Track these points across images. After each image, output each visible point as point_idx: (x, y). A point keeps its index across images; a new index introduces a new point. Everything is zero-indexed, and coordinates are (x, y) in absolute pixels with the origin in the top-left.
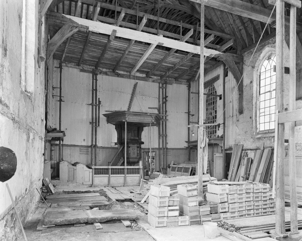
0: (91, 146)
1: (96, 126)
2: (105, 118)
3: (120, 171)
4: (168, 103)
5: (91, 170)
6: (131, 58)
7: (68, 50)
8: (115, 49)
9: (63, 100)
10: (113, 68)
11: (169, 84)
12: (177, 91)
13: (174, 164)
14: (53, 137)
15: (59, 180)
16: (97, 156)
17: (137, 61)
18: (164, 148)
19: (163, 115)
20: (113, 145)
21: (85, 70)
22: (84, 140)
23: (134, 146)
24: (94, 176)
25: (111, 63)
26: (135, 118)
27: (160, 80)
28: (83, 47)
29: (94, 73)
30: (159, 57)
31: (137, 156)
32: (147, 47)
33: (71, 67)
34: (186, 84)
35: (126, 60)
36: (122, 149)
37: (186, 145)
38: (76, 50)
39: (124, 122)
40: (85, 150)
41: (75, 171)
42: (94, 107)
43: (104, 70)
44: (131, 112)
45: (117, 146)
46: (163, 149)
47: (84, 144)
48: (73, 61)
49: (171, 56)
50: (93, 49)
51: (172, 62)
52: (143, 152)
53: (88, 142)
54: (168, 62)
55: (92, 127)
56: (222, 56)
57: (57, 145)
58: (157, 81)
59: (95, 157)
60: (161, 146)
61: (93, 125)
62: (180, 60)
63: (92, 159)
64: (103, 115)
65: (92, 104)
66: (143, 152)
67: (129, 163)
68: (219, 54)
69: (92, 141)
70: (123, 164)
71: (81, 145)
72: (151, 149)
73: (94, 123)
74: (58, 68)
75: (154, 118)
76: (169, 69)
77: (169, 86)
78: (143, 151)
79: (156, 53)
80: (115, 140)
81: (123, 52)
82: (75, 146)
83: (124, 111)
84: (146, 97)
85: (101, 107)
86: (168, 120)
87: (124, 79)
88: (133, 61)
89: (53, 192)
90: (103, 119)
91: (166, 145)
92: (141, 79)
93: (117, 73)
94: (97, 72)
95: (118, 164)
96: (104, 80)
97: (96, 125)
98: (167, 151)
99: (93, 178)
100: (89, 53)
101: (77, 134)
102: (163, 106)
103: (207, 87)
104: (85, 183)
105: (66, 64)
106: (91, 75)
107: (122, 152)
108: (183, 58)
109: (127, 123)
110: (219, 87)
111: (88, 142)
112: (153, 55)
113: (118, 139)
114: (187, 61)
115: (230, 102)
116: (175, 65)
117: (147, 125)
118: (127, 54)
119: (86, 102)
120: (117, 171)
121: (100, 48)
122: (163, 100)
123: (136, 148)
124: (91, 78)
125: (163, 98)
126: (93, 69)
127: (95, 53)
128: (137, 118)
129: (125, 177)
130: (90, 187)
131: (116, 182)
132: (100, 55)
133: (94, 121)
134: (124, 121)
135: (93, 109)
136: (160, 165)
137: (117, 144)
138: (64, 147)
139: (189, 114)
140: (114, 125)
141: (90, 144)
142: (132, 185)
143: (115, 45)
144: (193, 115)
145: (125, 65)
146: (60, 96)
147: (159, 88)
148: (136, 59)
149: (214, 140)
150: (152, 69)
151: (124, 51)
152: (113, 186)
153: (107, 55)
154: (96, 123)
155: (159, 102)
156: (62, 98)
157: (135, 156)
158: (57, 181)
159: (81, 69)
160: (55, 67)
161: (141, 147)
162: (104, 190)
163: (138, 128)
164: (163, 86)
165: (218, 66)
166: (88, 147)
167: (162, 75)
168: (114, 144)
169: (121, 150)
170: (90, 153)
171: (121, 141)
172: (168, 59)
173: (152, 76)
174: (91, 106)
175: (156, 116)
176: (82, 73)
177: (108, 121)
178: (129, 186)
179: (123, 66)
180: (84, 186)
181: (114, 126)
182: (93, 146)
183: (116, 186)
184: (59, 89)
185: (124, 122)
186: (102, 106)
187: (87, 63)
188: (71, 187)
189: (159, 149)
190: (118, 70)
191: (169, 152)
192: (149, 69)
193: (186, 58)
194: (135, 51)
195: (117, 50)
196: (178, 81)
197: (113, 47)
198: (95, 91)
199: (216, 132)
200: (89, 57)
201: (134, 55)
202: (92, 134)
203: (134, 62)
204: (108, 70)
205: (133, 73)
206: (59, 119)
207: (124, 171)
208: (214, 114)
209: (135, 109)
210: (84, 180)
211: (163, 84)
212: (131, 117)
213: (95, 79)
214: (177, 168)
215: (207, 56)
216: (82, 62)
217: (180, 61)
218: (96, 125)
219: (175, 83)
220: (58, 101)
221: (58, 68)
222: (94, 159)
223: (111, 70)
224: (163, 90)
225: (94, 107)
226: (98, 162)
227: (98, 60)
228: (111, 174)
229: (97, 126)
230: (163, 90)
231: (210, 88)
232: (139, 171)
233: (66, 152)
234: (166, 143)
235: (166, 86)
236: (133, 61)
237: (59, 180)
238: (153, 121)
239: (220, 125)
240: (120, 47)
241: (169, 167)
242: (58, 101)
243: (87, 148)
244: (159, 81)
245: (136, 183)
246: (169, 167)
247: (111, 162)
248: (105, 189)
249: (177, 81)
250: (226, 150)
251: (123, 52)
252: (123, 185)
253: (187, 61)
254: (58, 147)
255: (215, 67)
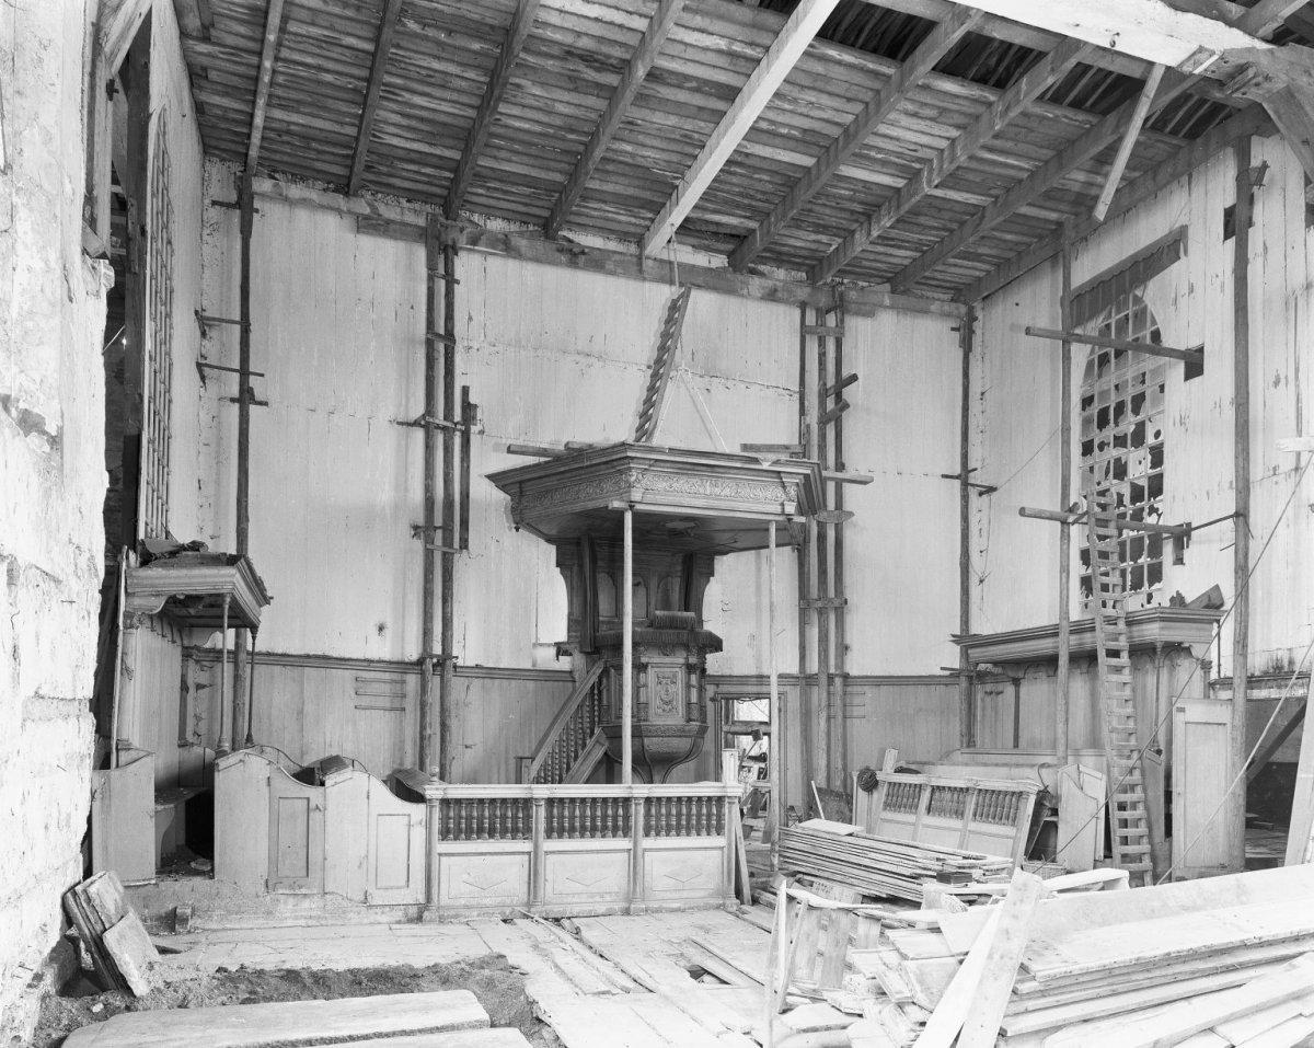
0: (420, 662)
1: (451, 545)
2: (500, 497)
3: (604, 817)
4: (850, 422)
5: (417, 811)
6: (662, 134)
7: (280, 79)
8: (569, 53)
9: (259, 396)
10: (546, 214)
11: (857, 314)
12: (896, 351)
13: (900, 770)
14: (173, 590)
15: (210, 874)
16: (453, 723)
17: (691, 148)
18: (831, 678)
19: (839, 475)
20: (546, 659)
21: (389, 222)
22: (381, 629)
23: (667, 660)
24: (442, 847)
25: (534, 173)
26: (686, 487)
27: (808, 290)
28: (369, 47)
29: (438, 238)
30: (830, 112)
31: (689, 720)
32: (768, 30)
33: (304, 202)
34: (949, 315)
35: (629, 148)
36: (600, 678)
37: (952, 658)
38: (329, 78)
39: (620, 514)
40: (386, 688)
41: (315, 816)
42: (440, 438)
43: (496, 225)
44: (659, 450)
45: (565, 663)
46: (823, 680)
47: (382, 649)
48: (318, 165)
49: (910, 107)
50: (436, 65)
51: (899, 155)
52: (713, 700)
53: (401, 638)
54: (880, 150)
55: (429, 554)
56: (1264, 61)
57: (217, 654)
58: (790, 292)
59: (444, 726)
60: (813, 666)
61: (429, 540)
62: (954, 133)
63: (422, 738)
64: (491, 477)
65: (425, 424)
66: (713, 700)
67: (651, 765)
68: (1250, 50)
69: (427, 633)
70: (608, 770)
71: (361, 657)
72: (774, 679)
73: (439, 533)
74: (228, 206)
75: (793, 491)
76: (872, 204)
77: (857, 326)
78: (710, 690)
79: (817, 84)
80: (556, 626)
81: (611, 79)
82: (325, 661)
83: (623, 444)
84: (729, 384)
85: (475, 440)
86: (851, 514)
87: (611, 280)
88: (665, 156)
89: (139, 986)
90: (487, 497)
91: (841, 663)
92: (700, 281)
93: (570, 241)
94: (452, 235)
95: (575, 766)
96: (498, 288)
97: (448, 541)
98: (845, 693)
99: (435, 859)
100: (407, 96)
101: (338, 602)
102: (823, 437)
103: (1093, 316)
104: (378, 898)
105: (275, 185)
106: (421, 253)
107: (600, 700)
108: (977, 118)
109: (639, 518)
110: (1183, 302)
111: (401, 638)
112: (795, 101)
113: (573, 623)
114: (998, 143)
115: (1276, 383)
116: (913, 176)
117: (743, 540)
118: (642, 99)
119: (388, 410)
120: (583, 817)
121: (476, 46)
122: (822, 404)
123: (681, 674)
124: (423, 271)
125: (823, 394)
126: (433, 219)
127: (448, 95)
128: (693, 489)
129: (634, 857)
130: (410, 921)
131: (578, 888)
132: (472, 113)
133: (438, 521)
134: (616, 504)
135: (429, 448)
136: (809, 774)
137: (567, 653)
138: (261, 671)
139: (965, 485)
140: (549, 540)
141: (413, 653)
142: (675, 905)
143: (570, 23)
144: (991, 490)
145: (619, 189)
146: (244, 372)
147: (804, 331)
148: (687, 139)
149: (1163, 620)
150: (768, 215)
151: (623, 68)
152: (556, 911)
153: (516, 111)
154: (447, 529)
155: (802, 411)
156: (253, 381)
157: (676, 719)
158: (197, 881)
159: (366, 218)
160: (214, 203)
161: (704, 670)
162: (511, 961)
163: (686, 551)
164: (821, 322)
165: (1175, 177)
166: (402, 666)
167: (820, 260)
168: (553, 651)
169: (593, 688)
170: (411, 704)
171: (593, 638)
172: (883, 129)
173: (762, 268)
174: (419, 434)
175: (807, 476)
176: (367, 242)
177: (521, 518)
178: (658, 910)
179: (603, 197)
180: (372, 916)
181: (552, 549)
182: (429, 665)
183: (576, 910)
184: (237, 329)
185: (620, 514)
186: (482, 432)
187: (397, 182)
188: (289, 923)
189: (806, 680)
190: (572, 225)
191: (857, 700)
192: (754, 213)
193: (1007, 109)
194: (690, 69)
195: (581, 67)
196: (906, 292)
197: (558, 37)
198: (441, 347)
199: (1156, 574)
200: (409, 128)
201: (678, 104)
202: (428, 594)
203: (675, 158)
204: (514, 227)
205: (657, 245)
206: (239, 501)
207: (627, 817)
208: (1139, 470)
209: (671, 433)
210: (372, 877)
211: (822, 313)
212: (661, 485)
213: (442, 275)
214: (926, 796)
215: (1168, 68)
216: (368, 168)
217: (953, 141)
218: (448, 541)
219: (892, 307)
220: (233, 400)
221: (228, 206)
222: (436, 740)
223: (531, 228)
224: (822, 342)
225: (440, 438)
226: (462, 760)
227: (457, 155)
228: (549, 834)
229: (456, 545)
230: (822, 342)
231: (1113, 322)
232: (720, 817)
233: (273, 694)
234: (844, 649)
235: (841, 323)
236: (665, 156)
237: (210, 874)
238: (791, 508)
239: (1194, 534)
240: (600, 39)
241: (870, 784)
242: (233, 400)
243: (395, 676)
244: (803, 293)
245: (702, 894)
246: (870, 784)
247: (533, 759)
248: (515, 946)
249: (903, 293)
250: (1253, 681)
251: (611, 79)
252: (625, 905)
253: (998, 143)
254: (228, 668)
255: (1161, 178)
